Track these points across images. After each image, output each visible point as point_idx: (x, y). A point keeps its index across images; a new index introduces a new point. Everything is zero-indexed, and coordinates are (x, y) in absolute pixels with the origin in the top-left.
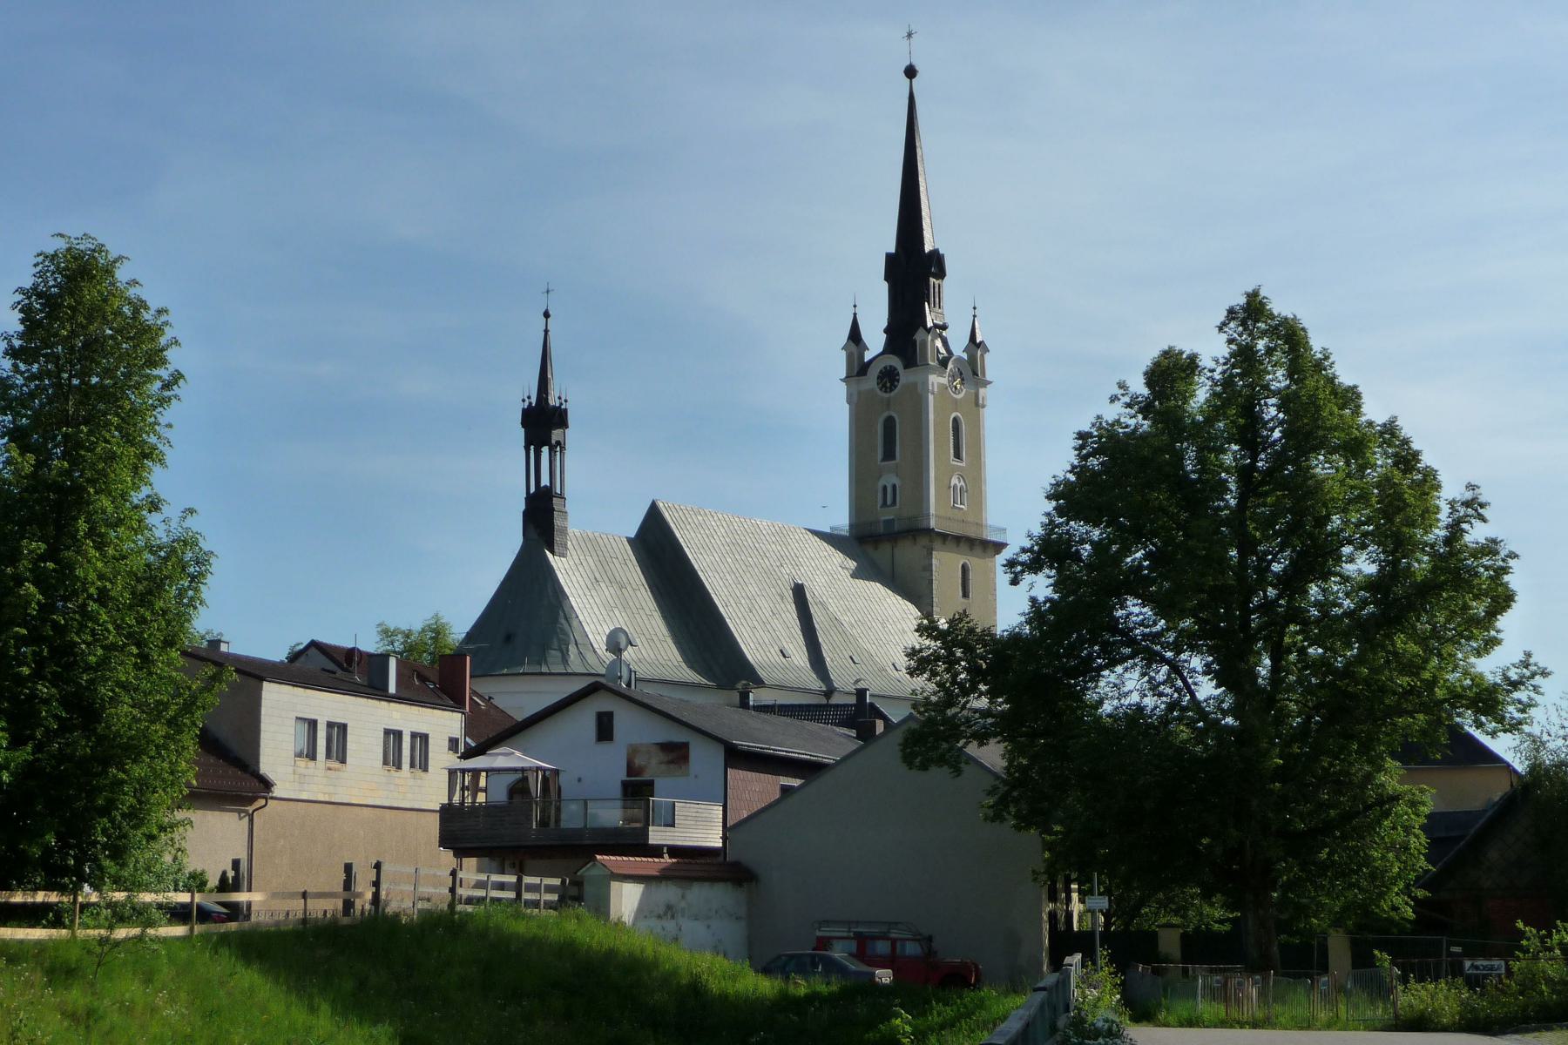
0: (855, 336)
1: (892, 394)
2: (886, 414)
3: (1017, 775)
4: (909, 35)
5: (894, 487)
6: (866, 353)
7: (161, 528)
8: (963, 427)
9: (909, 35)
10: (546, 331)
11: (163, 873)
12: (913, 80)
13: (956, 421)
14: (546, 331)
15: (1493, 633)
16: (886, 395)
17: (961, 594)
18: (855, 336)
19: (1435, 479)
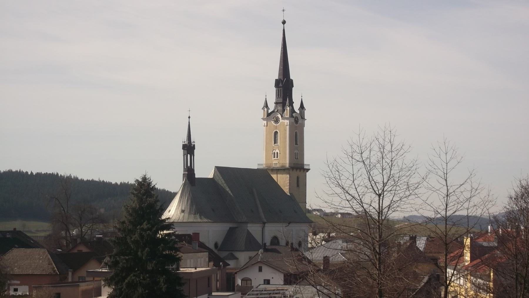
0: (266, 106)
1: (278, 125)
2: (275, 130)
3: (147, 291)
4: (283, 10)
5: (277, 153)
6: (269, 110)
7: (80, 179)
8: (298, 134)
9: (283, 10)
10: (189, 122)
11: (388, 267)
12: (285, 25)
13: (296, 133)
14: (189, 122)
15: (511, 211)
16: (276, 125)
17: (296, 185)
18: (266, 106)
19: (294, 283)
